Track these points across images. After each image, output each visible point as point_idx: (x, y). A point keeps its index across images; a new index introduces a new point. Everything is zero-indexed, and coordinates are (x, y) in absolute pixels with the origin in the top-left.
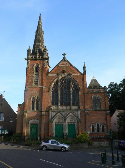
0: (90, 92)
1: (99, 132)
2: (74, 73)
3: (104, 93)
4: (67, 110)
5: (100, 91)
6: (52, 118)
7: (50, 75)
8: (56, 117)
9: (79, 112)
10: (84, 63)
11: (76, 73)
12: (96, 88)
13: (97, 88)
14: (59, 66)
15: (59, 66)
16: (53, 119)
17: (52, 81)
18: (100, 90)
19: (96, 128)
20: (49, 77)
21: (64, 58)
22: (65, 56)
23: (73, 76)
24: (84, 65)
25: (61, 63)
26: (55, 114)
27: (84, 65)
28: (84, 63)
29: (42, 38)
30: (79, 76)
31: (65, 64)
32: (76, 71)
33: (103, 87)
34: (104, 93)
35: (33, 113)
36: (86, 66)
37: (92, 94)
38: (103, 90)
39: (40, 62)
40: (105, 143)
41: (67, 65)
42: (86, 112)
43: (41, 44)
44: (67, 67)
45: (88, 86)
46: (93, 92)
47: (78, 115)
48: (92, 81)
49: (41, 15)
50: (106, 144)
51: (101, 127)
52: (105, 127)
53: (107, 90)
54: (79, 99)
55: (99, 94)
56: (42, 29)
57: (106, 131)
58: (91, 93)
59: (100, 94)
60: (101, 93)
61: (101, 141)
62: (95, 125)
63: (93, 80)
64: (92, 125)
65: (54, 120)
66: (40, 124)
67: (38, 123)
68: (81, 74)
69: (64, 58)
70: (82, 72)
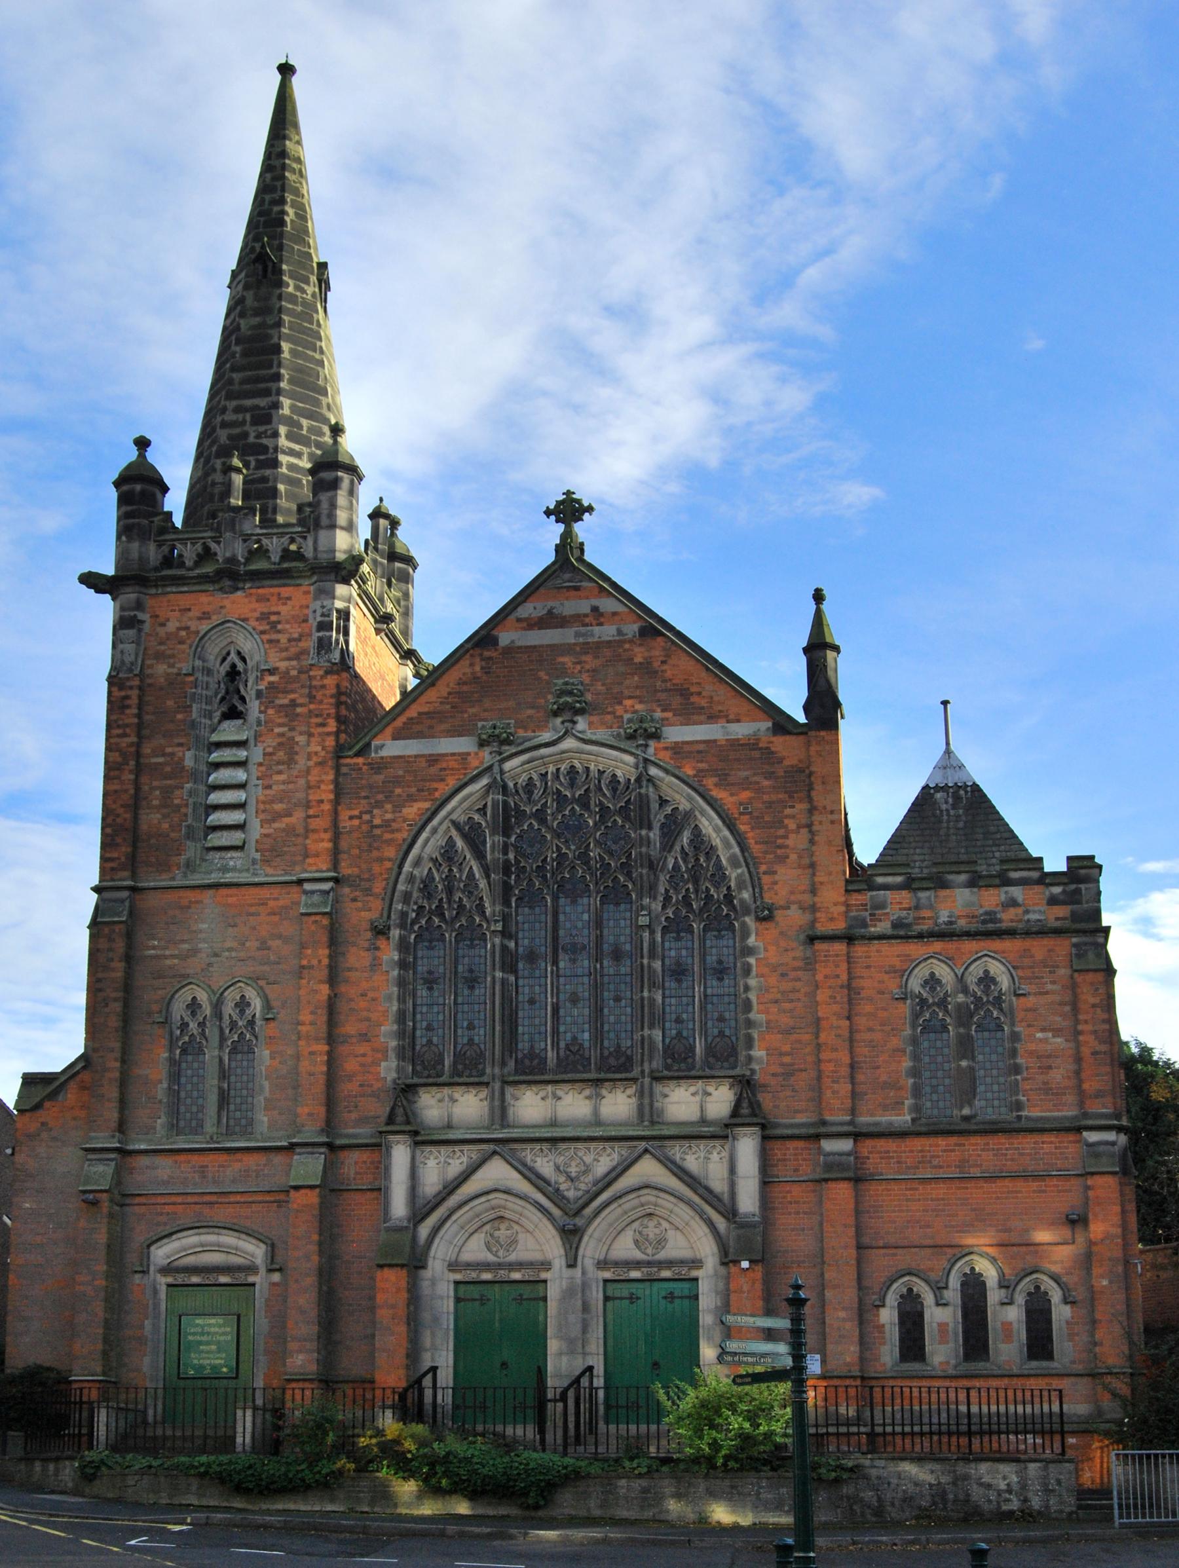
0: (883, 927)
1: (916, 1366)
2: (689, 713)
3: (1057, 932)
4: (598, 1132)
5: (1012, 913)
6: (419, 1213)
7: (390, 748)
8: (460, 1206)
9: (747, 1147)
10: (818, 597)
11: (712, 718)
12: (963, 878)
13: (972, 884)
14: (505, 637)
15: (505, 637)
16: (424, 1231)
17: (412, 811)
18: (1013, 903)
19: (942, 1327)
20: (380, 766)
21: (568, 549)
22: (580, 529)
23: (678, 750)
24: (818, 622)
25: (528, 610)
26: (457, 1163)
27: (818, 622)
28: (818, 597)
29: (311, 338)
30: (751, 744)
31: (578, 619)
32: (710, 687)
33: (1055, 864)
34: (1057, 932)
35: (195, 1159)
36: (836, 632)
37: (916, 949)
38: (1053, 901)
39: (263, 608)
40: (1023, 1486)
41: (607, 632)
42: (828, 1145)
43: (286, 411)
44: (599, 645)
45: (867, 851)
46: (925, 927)
47: (732, 1185)
48: (924, 803)
49: (296, 81)
50: (1047, 1491)
51: (1015, 1314)
52: (1061, 1313)
53: (363, 1442)
54: (748, 1005)
55: (997, 944)
56: (302, 233)
57: (1065, 1349)
58: (902, 932)
59: (1007, 944)
60: (1028, 934)
61: (970, 1457)
62: (939, 1288)
63: (937, 788)
64: (898, 1287)
65: (435, 1231)
66: (276, 1277)
67: (252, 1269)
68: (781, 722)
69: (568, 549)
70: (538, 1247)
